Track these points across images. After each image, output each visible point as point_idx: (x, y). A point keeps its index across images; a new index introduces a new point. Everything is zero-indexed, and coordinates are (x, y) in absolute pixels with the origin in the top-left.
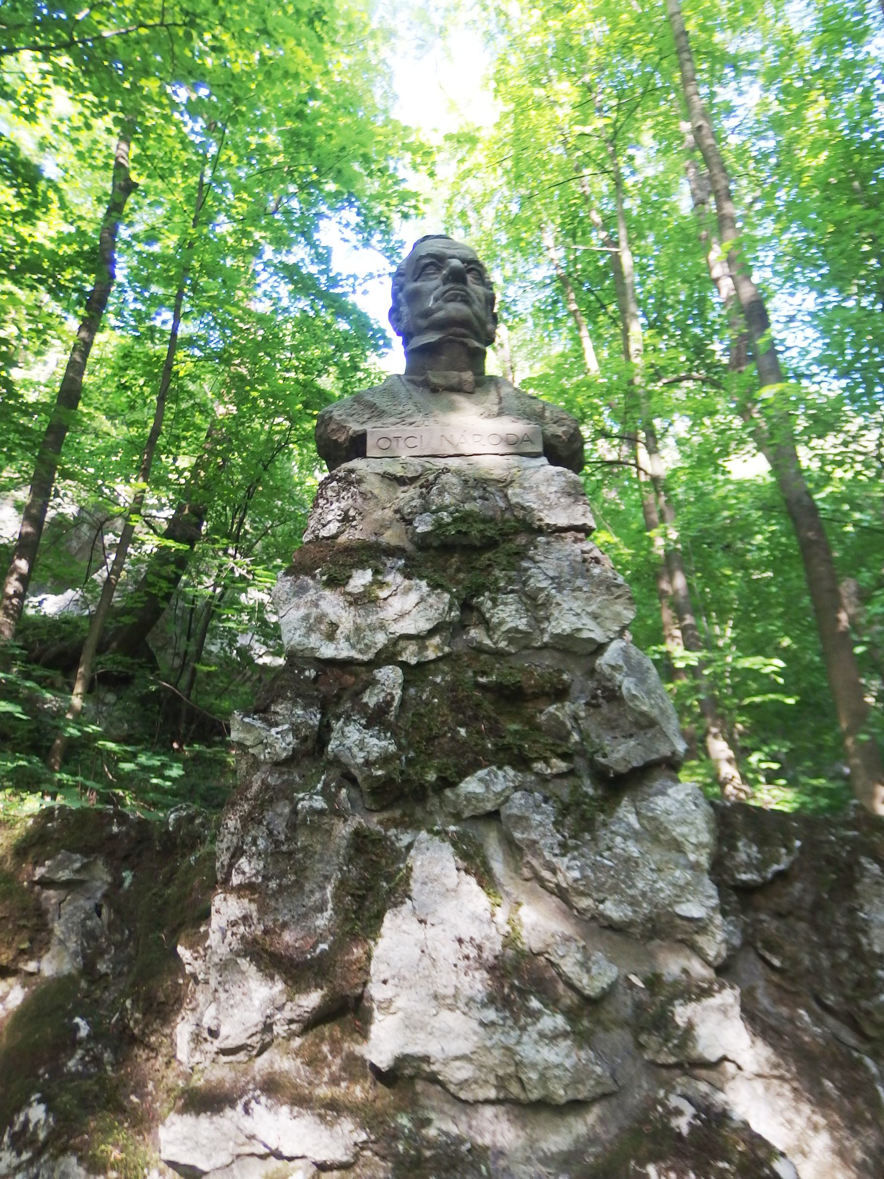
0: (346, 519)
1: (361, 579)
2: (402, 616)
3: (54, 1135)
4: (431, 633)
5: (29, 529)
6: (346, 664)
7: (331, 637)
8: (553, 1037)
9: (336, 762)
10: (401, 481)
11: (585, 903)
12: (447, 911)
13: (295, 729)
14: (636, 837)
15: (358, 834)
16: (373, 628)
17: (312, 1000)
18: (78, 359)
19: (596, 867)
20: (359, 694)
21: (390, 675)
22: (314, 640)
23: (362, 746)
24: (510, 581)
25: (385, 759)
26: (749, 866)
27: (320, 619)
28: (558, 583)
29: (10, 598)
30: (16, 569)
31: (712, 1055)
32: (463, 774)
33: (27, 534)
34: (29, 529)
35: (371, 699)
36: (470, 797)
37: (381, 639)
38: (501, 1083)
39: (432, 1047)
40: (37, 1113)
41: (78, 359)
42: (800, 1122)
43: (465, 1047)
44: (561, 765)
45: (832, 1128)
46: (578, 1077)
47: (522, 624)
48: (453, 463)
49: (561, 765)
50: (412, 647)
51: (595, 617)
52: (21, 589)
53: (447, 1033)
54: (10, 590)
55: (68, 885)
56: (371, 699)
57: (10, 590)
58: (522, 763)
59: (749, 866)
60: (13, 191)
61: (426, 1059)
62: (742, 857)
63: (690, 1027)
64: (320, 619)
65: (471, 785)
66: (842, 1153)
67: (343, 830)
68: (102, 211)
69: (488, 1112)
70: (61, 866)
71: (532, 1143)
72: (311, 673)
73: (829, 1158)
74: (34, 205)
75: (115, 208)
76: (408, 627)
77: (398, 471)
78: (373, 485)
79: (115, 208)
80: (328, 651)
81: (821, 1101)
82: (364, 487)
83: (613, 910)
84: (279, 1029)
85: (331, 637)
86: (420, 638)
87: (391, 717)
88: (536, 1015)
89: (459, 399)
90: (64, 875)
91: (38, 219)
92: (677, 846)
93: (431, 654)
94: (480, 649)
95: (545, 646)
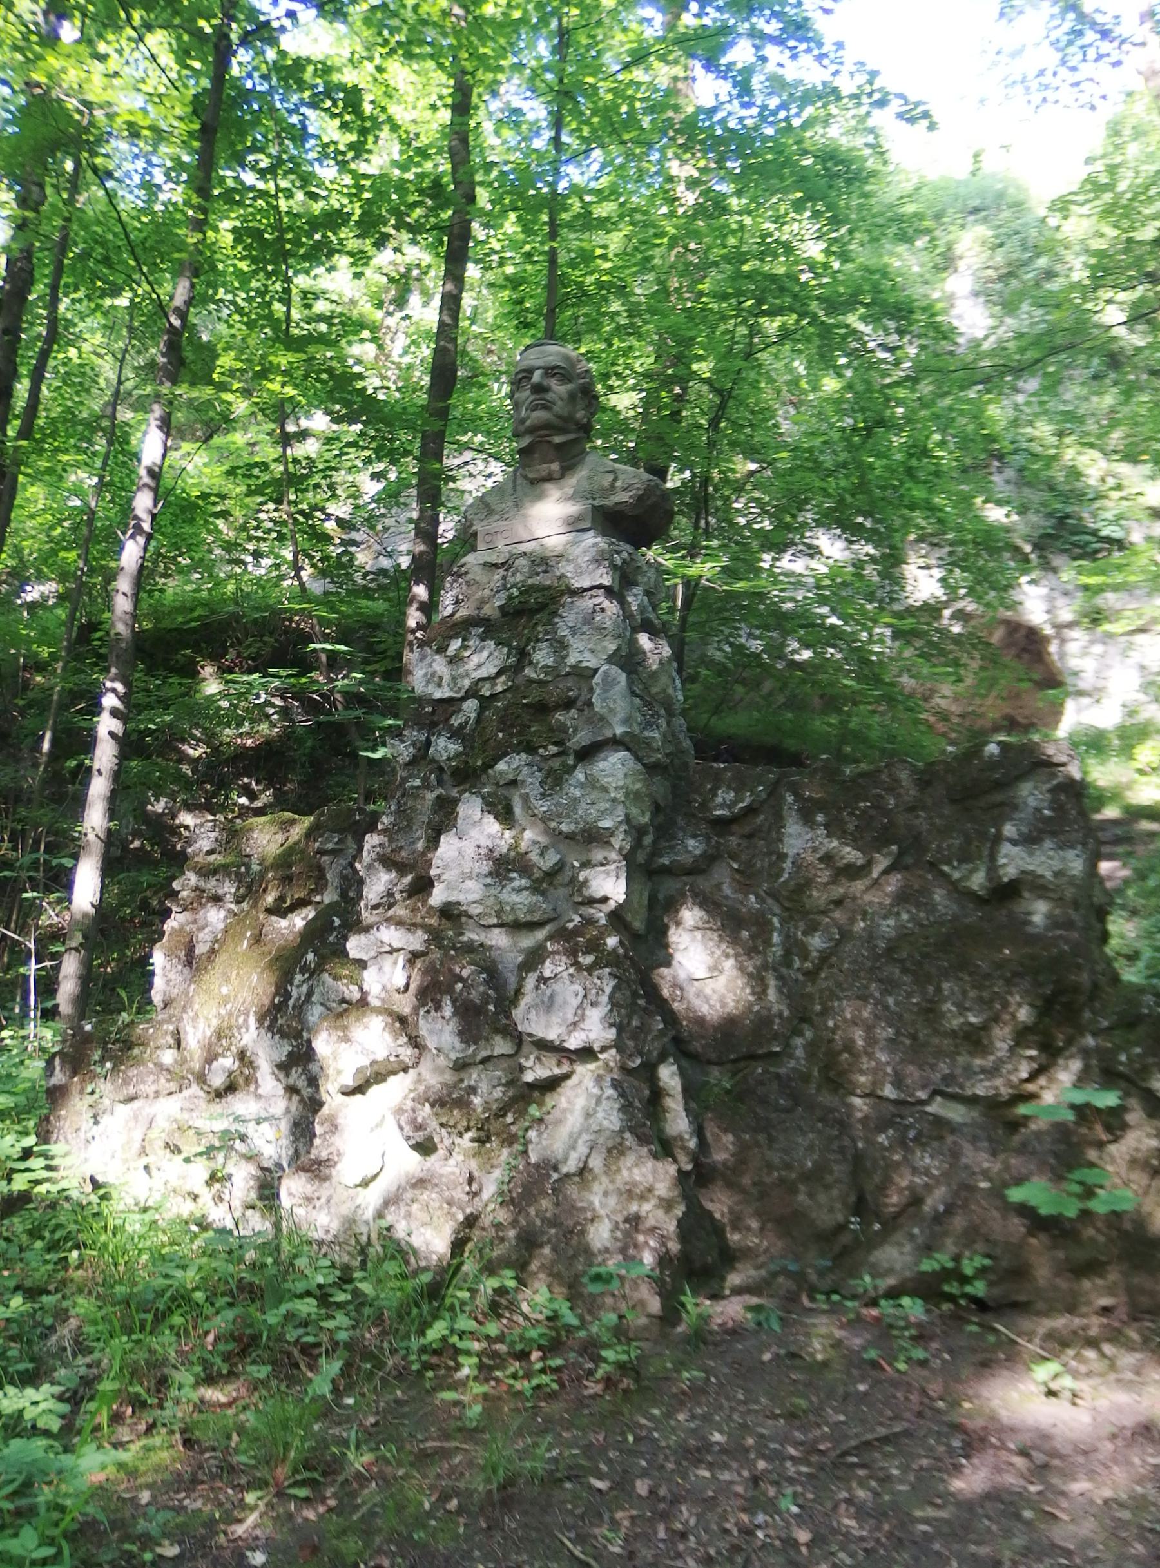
0: (457, 602)
1: (456, 644)
2: (480, 666)
3: (318, 965)
4: (499, 674)
5: (422, 548)
6: (449, 701)
7: (439, 685)
8: (520, 890)
9: (433, 761)
10: (496, 566)
11: (553, 824)
12: (474, 833)
13: (414, 744)
14: (582, 785)
15: (438, 797)
16: (462, 677)
17: (408, 879)
18: (448, 320)
19: (557, 804)
20: (448, 719)
21: (471, 705)
22: (431, 689)
23: (446, 749)
24: (547, 633)
25: (458, 755)
26: (723, 806)
27: (433, 674)
28: (573, 630)
29: (413, 632)
30: (414, 598)
31: (599, 894)
32: (497, 760)
33: (421, 553)
34: (422, 548)
35: (455, 721)
36: (501, 773)
37: (467, 683)
38: (498, 914)
39: (461, 898)
40: (310, 956)
41: (448, 320)
42: (718, 953)
43: (476, 897)
44: (553, 749)
45: (736, 956)
46: (531, 910)
47: (550, 661)
48: (523, 548)
49: (553, 749)
50: (488, 685)
51: (592, 651)
52: (423, 620)
53: (468, 891)
54: (412, 623)
55: (333, 852)
56: (455, 721)
57: (412, 623)
58: (531, 749)
59: (723, 806)
60: (337, 122)
61: (458, 903)
62: (719, 800)
63: (586, 881)
64: (433, 674)
65: (501, 766)
66: (741, 969)
67: (430, 796)
68: (445, 116)
69: (496, 931)
70: (327, 840)
71: (515, 944)
72: (429, 709)
73: (735, 972)
74: (363, 132)
75: (462, 106)
76: (483, 673)
77: (493, 559)
78: (477, 574)
79: (462, 106)
80: (438, 695)
81: (735, 941)
82: (469, 577)
83: (564, 828)
84: (398, 896)
85: (439, 685)
86: (491, 679)
87: (467, 730)
88: (512, 880)
89: (548, 486)
90: (329, 846)
91: (370, 152)
92: (605, 790)
93: (499, 688)
94: (531, 681)
95: (568, 674)
